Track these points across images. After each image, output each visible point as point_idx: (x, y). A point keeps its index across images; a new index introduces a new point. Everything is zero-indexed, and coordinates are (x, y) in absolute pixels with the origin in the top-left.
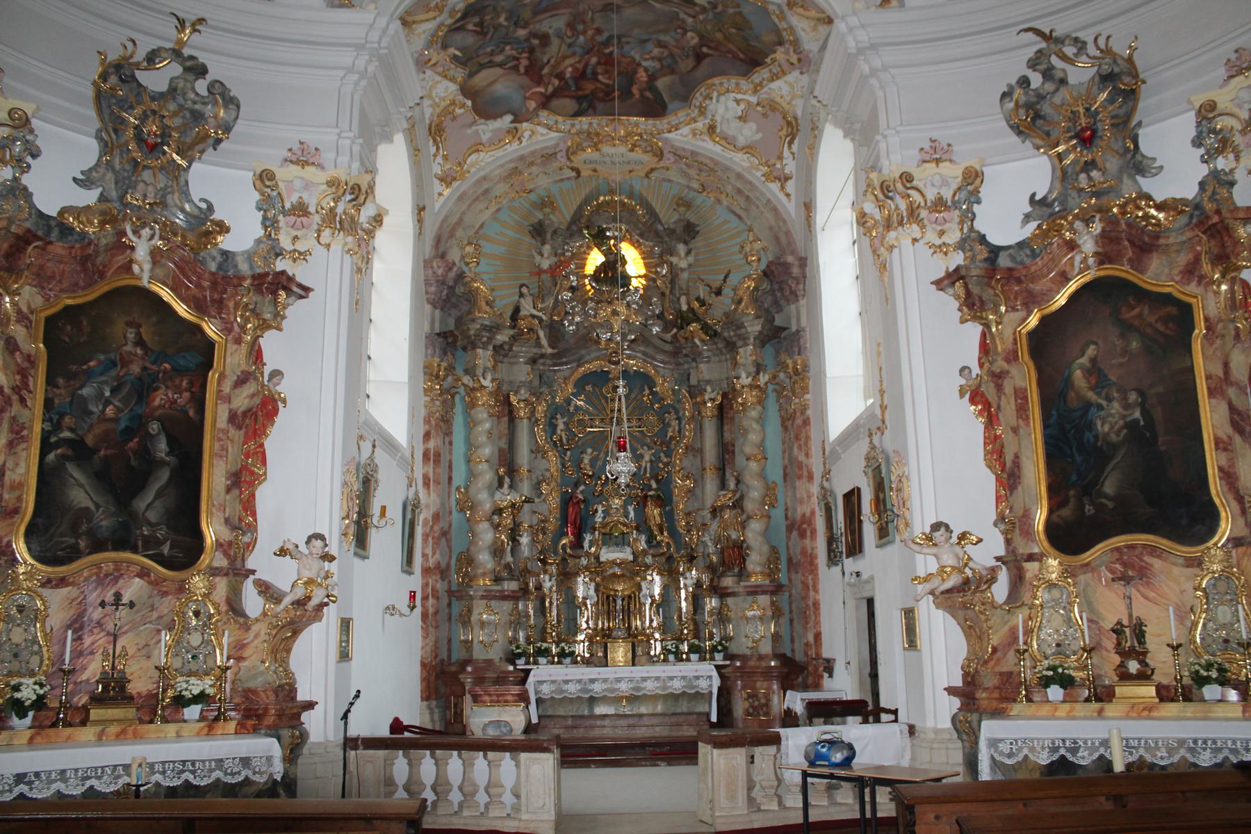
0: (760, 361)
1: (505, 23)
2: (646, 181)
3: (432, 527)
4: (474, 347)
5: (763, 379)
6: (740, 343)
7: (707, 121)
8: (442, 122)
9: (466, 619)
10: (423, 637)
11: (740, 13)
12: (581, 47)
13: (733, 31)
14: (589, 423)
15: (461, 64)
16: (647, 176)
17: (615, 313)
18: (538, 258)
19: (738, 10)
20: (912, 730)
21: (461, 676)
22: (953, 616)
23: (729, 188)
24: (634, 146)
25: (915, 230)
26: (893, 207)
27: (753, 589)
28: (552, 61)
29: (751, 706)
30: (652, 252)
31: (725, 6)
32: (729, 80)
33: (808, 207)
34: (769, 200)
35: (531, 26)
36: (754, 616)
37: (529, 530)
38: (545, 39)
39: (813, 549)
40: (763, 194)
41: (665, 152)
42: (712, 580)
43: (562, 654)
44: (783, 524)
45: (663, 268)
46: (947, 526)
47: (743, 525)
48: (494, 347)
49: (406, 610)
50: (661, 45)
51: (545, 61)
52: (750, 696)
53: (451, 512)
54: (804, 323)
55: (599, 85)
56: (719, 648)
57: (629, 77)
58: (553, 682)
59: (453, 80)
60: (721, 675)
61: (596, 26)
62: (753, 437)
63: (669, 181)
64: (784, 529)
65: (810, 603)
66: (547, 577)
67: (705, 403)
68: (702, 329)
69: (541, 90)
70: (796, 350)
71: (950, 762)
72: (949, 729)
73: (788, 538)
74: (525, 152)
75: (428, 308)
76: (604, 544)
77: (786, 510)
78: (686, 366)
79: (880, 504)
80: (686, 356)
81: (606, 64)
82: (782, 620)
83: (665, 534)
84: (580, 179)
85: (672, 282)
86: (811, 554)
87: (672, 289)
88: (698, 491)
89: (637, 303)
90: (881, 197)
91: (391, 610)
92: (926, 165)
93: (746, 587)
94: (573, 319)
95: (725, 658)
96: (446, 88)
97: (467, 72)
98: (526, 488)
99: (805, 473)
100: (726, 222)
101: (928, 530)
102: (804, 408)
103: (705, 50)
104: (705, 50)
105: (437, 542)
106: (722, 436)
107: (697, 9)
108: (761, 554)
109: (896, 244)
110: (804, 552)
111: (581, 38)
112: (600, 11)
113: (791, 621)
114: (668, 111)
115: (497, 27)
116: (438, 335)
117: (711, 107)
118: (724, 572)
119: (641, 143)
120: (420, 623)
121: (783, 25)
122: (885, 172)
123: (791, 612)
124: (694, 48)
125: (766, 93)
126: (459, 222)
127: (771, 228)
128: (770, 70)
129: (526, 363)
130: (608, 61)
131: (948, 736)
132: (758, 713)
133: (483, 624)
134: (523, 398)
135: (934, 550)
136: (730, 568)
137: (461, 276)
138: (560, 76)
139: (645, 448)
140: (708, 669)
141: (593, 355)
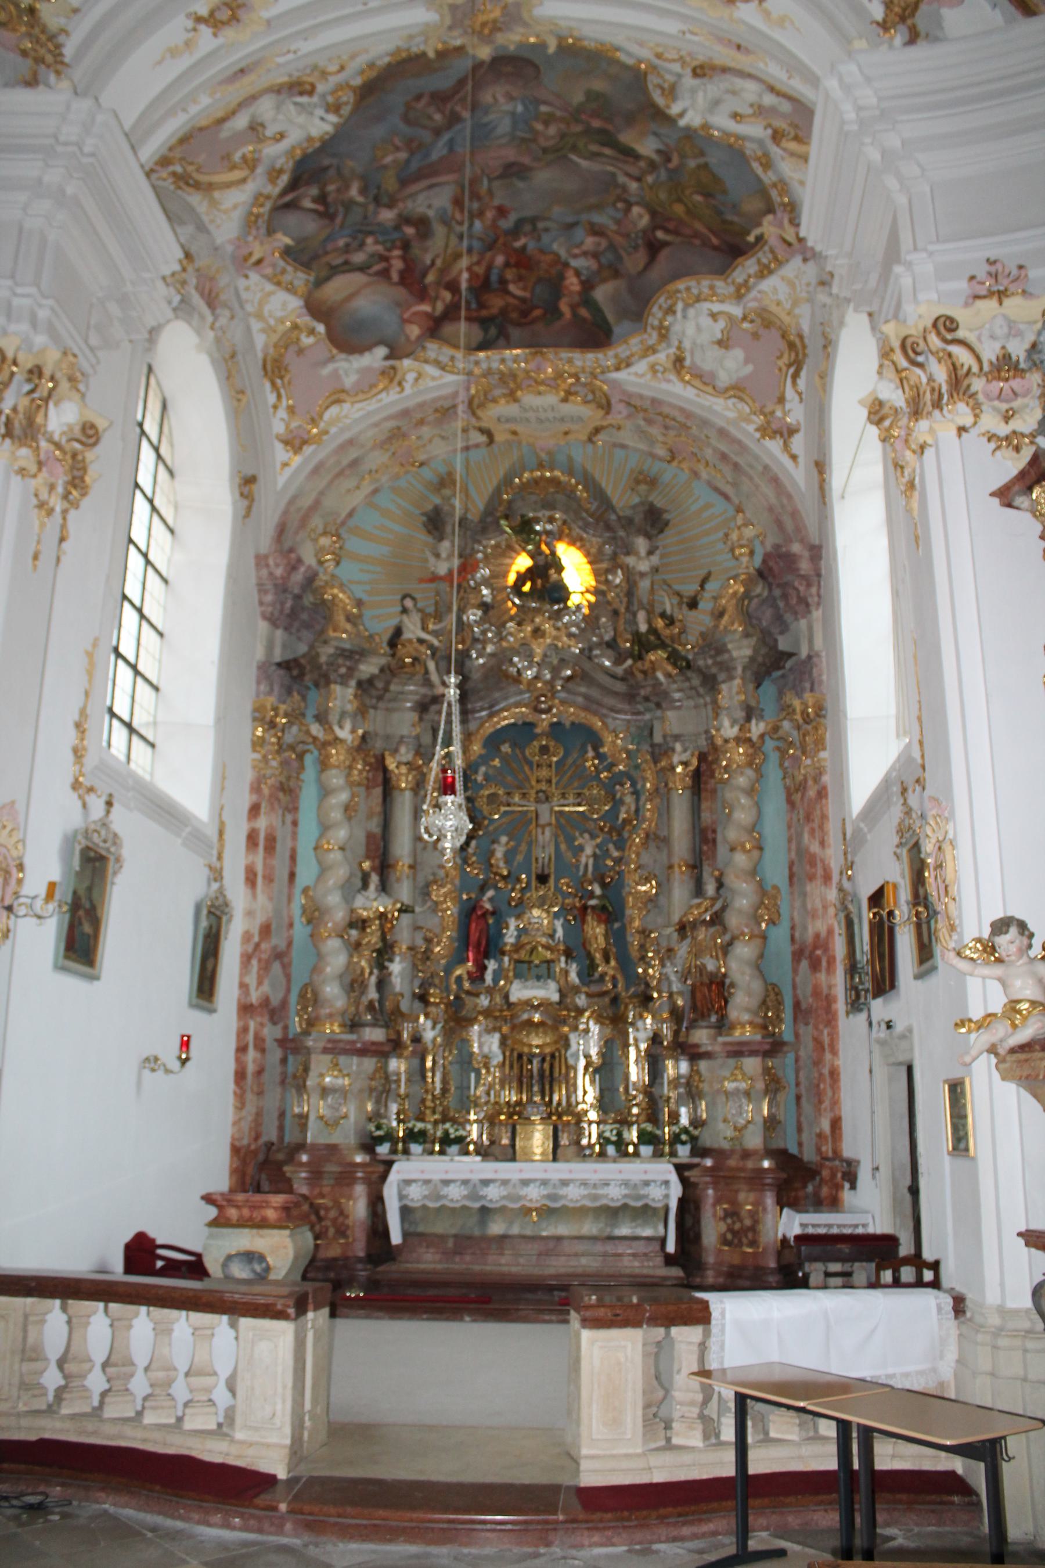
0: (753, 703)
1: (360, 199)
2: (590, 447)
3: (257, 946)
4: (328, 683)
5: (757, 728)
6: (722, 676)
7: (672, 351)
8: (281, 355)
9: (301, 1082)
10: (236, 1108)
11: (705, 166)
12: (480, 239)
13: (698, 198)
14: (504, 799)
15: (302, 264)
16: (590, 440)
17: (537, 632)
18: (432, 560)
19: (701, 161)
20: (959, 1305)
21: (286, 1168)
22: (1035, 1096)
23: (708, 453)
24: (569, 393)
25: (962, 412)
26: (924, 380)
27: (736, 1048)
28: (439, 262)
29: (730, 1229)
30: (600, 551)
31: (683, 156)
32: (699, 283)
33: (821, 466)
34: (766, 467)
35: (401, 205)
36: (737, 1090)
37: (409, 954)
38: (422, 225)
39: (830, 987)
40: (757, 458)
41: (613, 401)
42: (676, 1033)
43: (446, 1141)
44: (787, 950)
45: (615, 574)
46: (1022, 926)
47: (726, 949)
48: (360, 684)
49: (175, 1065)
50: (596, 231)
51: (428, 262)
52: (727, 1214)
53: (291, 925)
54: (819, 644)
55: (511, 300)
56: (684, 1137)
57: (555, 285)
58: (427, 1182)
59: (291, 289)
60: (684, 1181)
61: (497, 202)
62: (743, 816)
63: (623, 446)
64: (789, 957)
65: (826, 1071)
66: (429, 1024)
67: (673, 768)
68: (668, 659)
69: (426, 308)
70: (807, 685)
71: (1030, 1377)
72: (1027, 1311)
73: (795, 971)
74: (410, 404)
75: (263, 626)
76: (517, 976)
77: (793, 928)
78: (647, 716)
79: (920, 898)
80: (647, 699)
81: (517, 265)
82: (781, 1097)
83: (613, 963)
84: (494, 446)
85: (630, 594)
86: (828, 996)
87: (629, 603)
88: (662, 900)
89: (577, 626)
90: (903, 363)
91: (152, 1062)
92: (980, 303)
93: (725, 1044)
94: (484, 648)
95: (694, 1153)
96: (284, 304)
97: (312, 278)
98: (404, 892)
99: (820, 872)
100: (708, 506)
101: (986, 933)
102: (820, 772)
103: (660, 235)
104: (660, 235)
105: (265, 968)
106: (699, 818)
107: (642, 164)
108: (749, 994)
109: (930, 441)
110: (816, 993)
111: (478, 225)
112: (501, 177)
113: (798, 1098)
114: (614, 338)
115: (349, 205)
116: (279, 665)
117: (676, 328)
118: (695, 1020)
119: (578, 388)
120: (231, 1086)
121: (768, 178)
122: (910, 322)
123: (798, 1084)
124: (644, 232)
125: (755, 299)
126: (316, 504)
127: (771, 509)
128: (759, 261)
129: (412, 709)
130: (521, 261)
131: (1027, 1325)
132: (740, 1241)
133: (325, 1092)
134: (404, 759)
135: (998, 970)
136: (704, 1016)
137: (311, 579)
138: (453, 287)
139: (586, 836)
140: (665, 1170)
141: (512, 700)
